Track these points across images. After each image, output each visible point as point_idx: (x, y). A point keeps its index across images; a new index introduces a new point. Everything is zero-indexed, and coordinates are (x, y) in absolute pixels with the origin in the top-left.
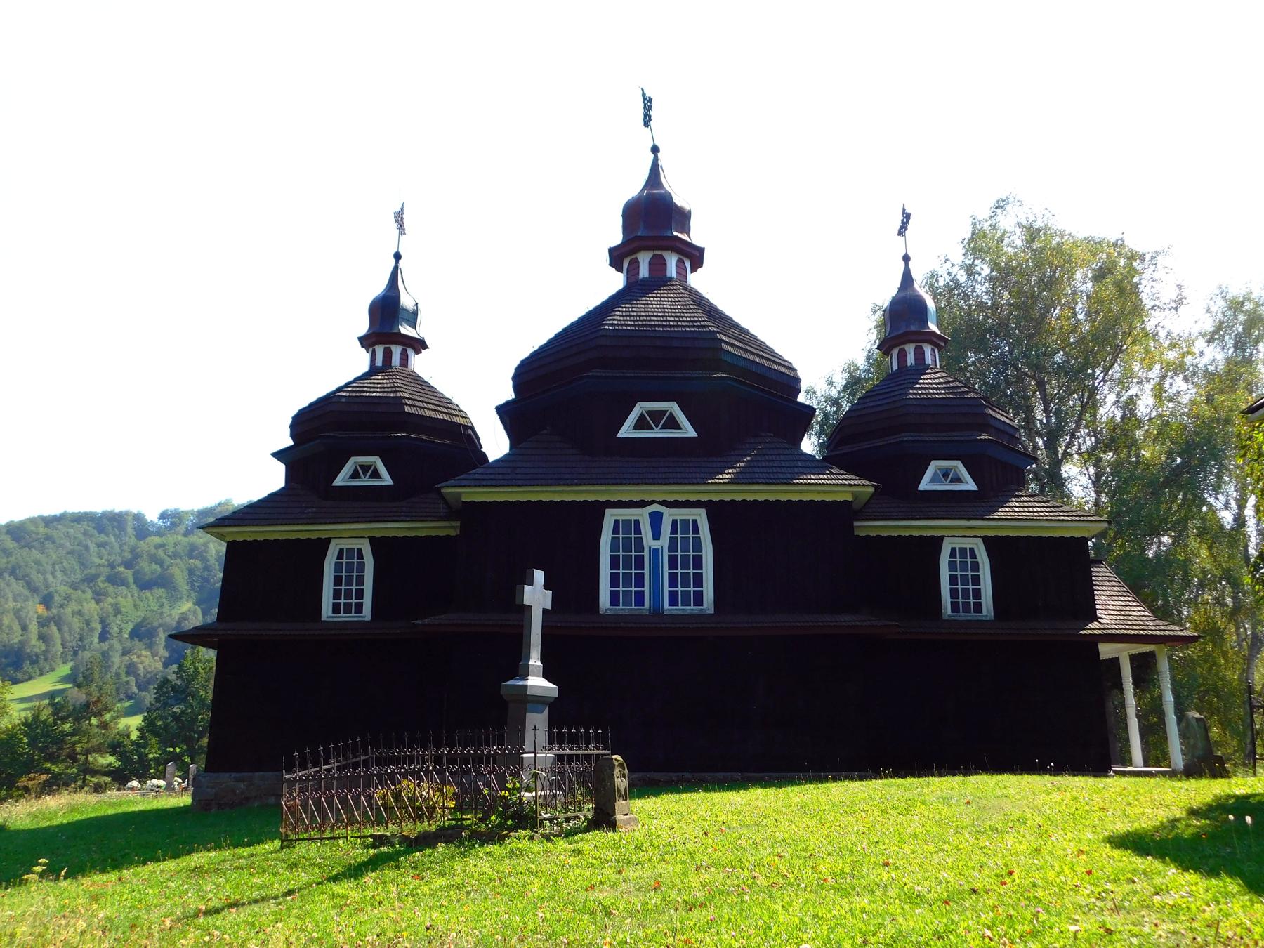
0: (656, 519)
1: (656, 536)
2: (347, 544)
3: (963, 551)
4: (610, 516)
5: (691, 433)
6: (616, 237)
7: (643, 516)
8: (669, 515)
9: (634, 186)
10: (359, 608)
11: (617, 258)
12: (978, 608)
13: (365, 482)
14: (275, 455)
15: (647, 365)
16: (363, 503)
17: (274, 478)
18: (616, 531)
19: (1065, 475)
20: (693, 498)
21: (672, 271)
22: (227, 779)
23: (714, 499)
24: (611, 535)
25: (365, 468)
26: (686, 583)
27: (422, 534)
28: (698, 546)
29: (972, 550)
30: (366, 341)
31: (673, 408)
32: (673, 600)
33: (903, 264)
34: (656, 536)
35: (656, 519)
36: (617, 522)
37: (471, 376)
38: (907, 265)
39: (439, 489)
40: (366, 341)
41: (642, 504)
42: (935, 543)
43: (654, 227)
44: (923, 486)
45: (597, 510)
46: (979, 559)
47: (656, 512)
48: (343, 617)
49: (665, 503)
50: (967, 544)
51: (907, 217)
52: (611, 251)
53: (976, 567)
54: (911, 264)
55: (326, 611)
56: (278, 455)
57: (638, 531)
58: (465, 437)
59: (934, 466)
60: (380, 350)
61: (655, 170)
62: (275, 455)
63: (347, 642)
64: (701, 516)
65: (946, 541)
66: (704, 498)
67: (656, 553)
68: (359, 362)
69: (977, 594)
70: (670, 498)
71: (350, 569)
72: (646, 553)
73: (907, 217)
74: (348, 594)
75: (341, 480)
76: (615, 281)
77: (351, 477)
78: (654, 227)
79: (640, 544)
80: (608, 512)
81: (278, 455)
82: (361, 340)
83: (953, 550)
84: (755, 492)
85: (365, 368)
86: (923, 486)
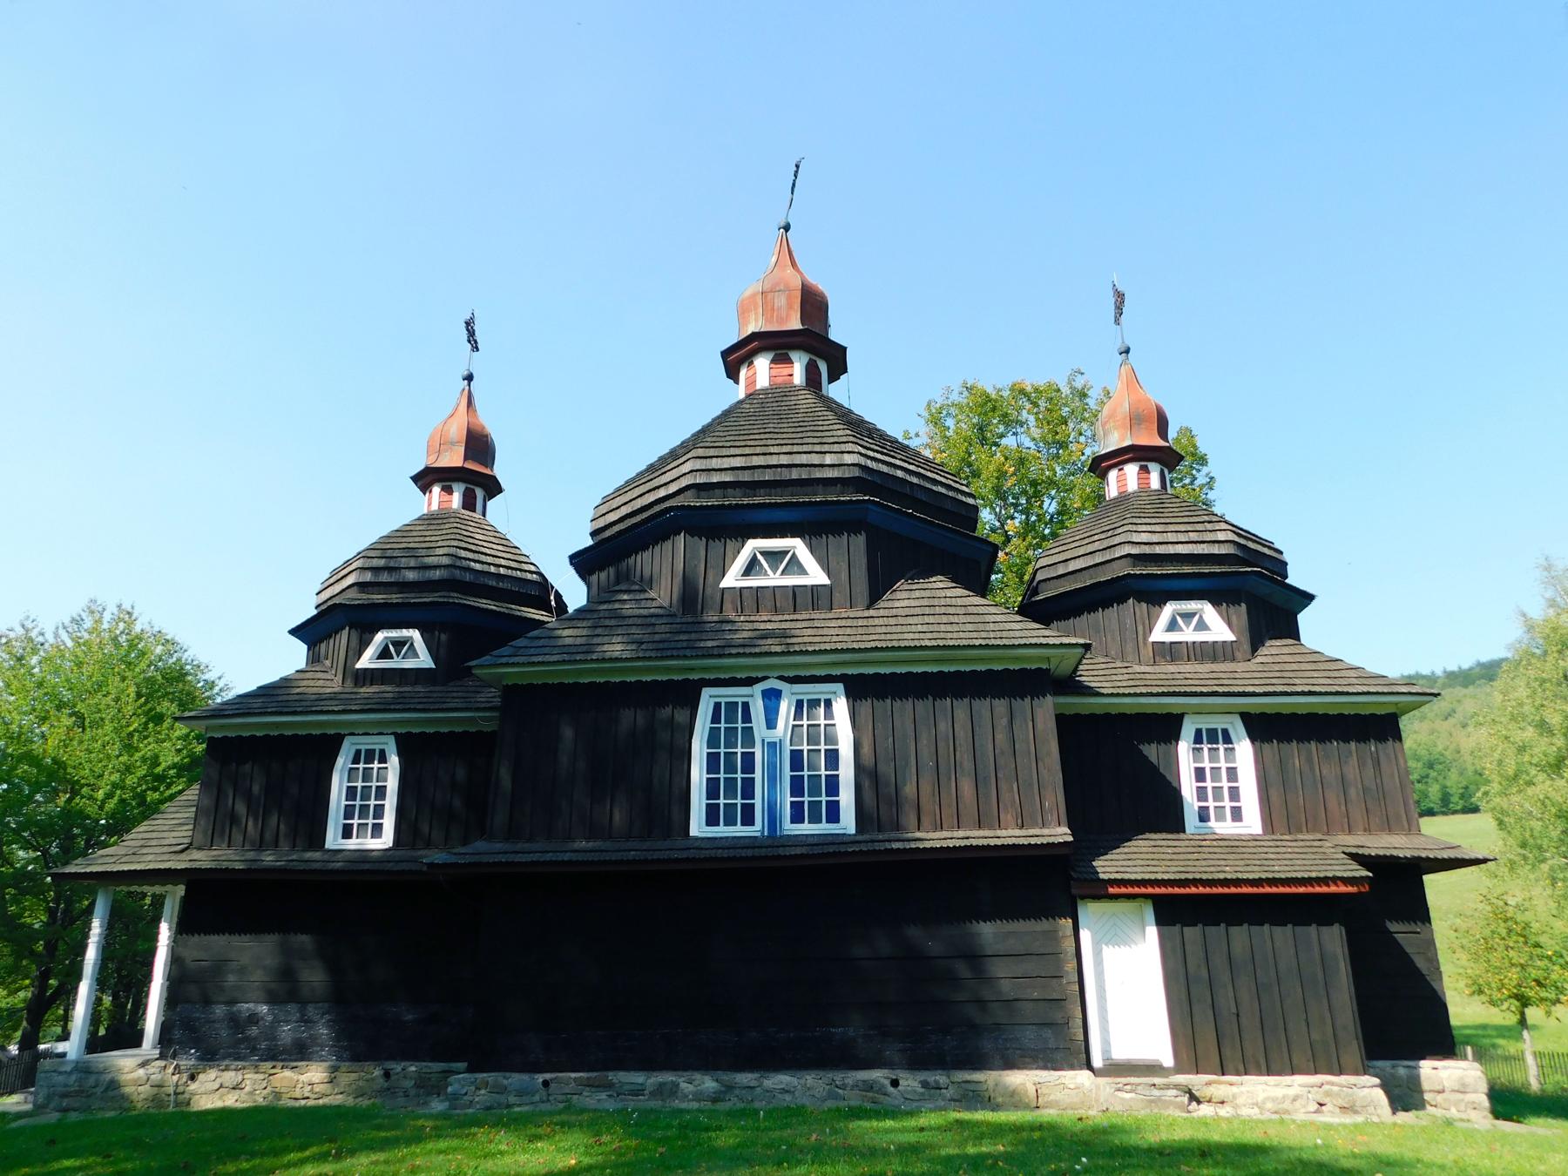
2: (365, 743)
10: (834, 814)
14: (294, 632)
18: (716, 718)
23: (659, 678)
24: (708, 725)
26: (731, 792)
32: (797, 817)
34: (771, 724)
36: (717, 706)
39: (470, 668)
47: (772, 690)
48: (722, 831)
55: (698, 827)
56: (1308, 598)
57: (747, 717)
58: (540, 592)
62: (294, 632)
63: (364, 874)
72: (758, 751)
74: (364, 810)
79: (748, 733)
80: (706, 693)
81: (1308, 598)
84: (668, 669)
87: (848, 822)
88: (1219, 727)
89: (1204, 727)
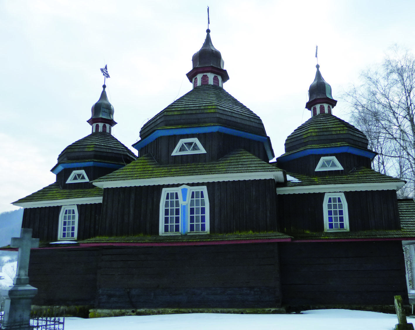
0: (184, 192)
1: (184, 200)
3: (335, 199)
4: (165, 192)
6: (190, 67)
9: (198, 47)
11: (191, 76)
12: (342, 226)
13: (79, 181)
15: (209, 119)
16: (189, 164)
17: (52, 179)
20: (201, 181)
21: (211, 82)
25: (79, 175)
28: (203, 203)
29: (339, 199)
34: (184, 200)
35: (184, 192)
37: (127, 133)
40: (91, 121)
41: (178, 185)
42: (320, 196)
43: (208, 62)
44: (317, 170)
45: (159, 188)
46: (342, 203)
49: (188, 184)
50: (337, 196)
52: (188, 75)
53: (341, 206)
57: (177, 198)
59: (323, 159)
61: (208, 40)
66: (206, 181)
67: (184, 207)
68: (88, 130)
69: (342, 219)
70: (191, 182)
72: (180, 208)
75: (176, 152)
76: (189, 87)
77: (74, 179)
78: (208, 62)
79: (177, 204)
83: (330, 199)
85: (90, 133)
86: (317, 170)
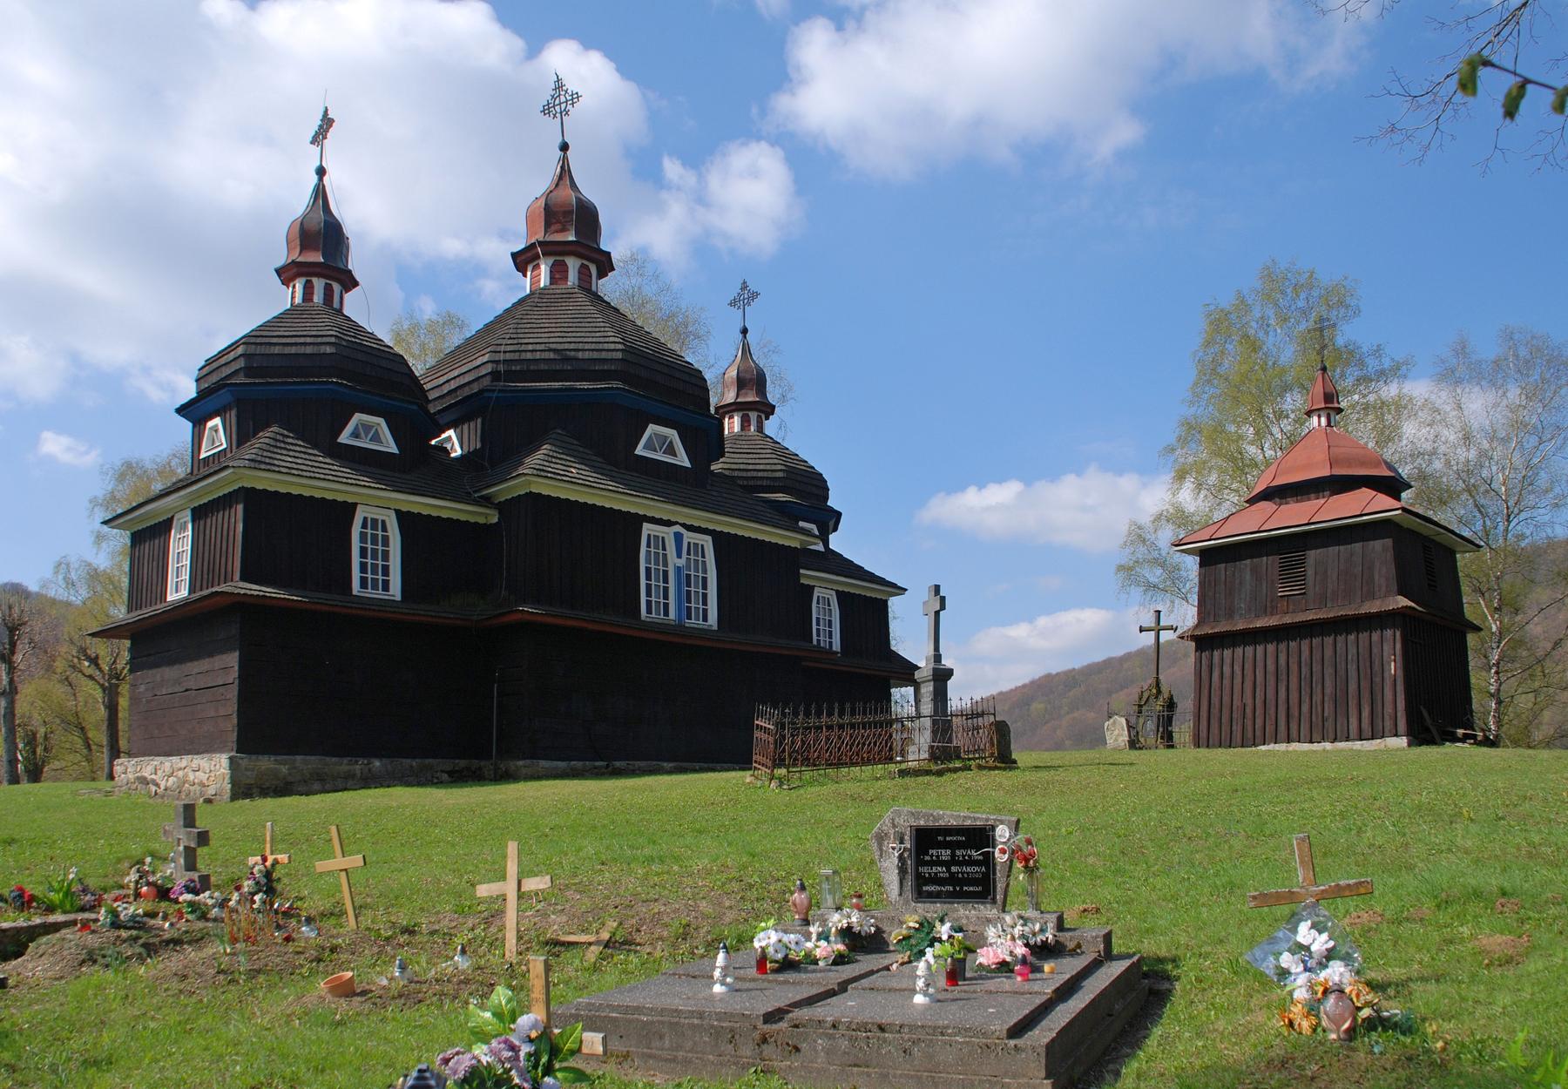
1: (679, 556)
5: (687, 464)
7: (668, 533)
8: (689, 537)
19: (1389, 633)
22: (266, 763)
27: (445, 515)
29: (383, 522)
30: (287, 274)
31: (672, 434)
33: (315, 179)
34: (679, 556)
38: (321, 180)
41: (669, 523)
46: (390, 534)
51: (327, 123)
54: (326, 179)
60: (299, 285)
63: (374, 622)
64: (707, 542)
65: (359, 508)
71: (375, 542)
73: (327, 123)
82: (279, 272)
87: (396, 590)
88: (380, 518)
89: (370, 516)
